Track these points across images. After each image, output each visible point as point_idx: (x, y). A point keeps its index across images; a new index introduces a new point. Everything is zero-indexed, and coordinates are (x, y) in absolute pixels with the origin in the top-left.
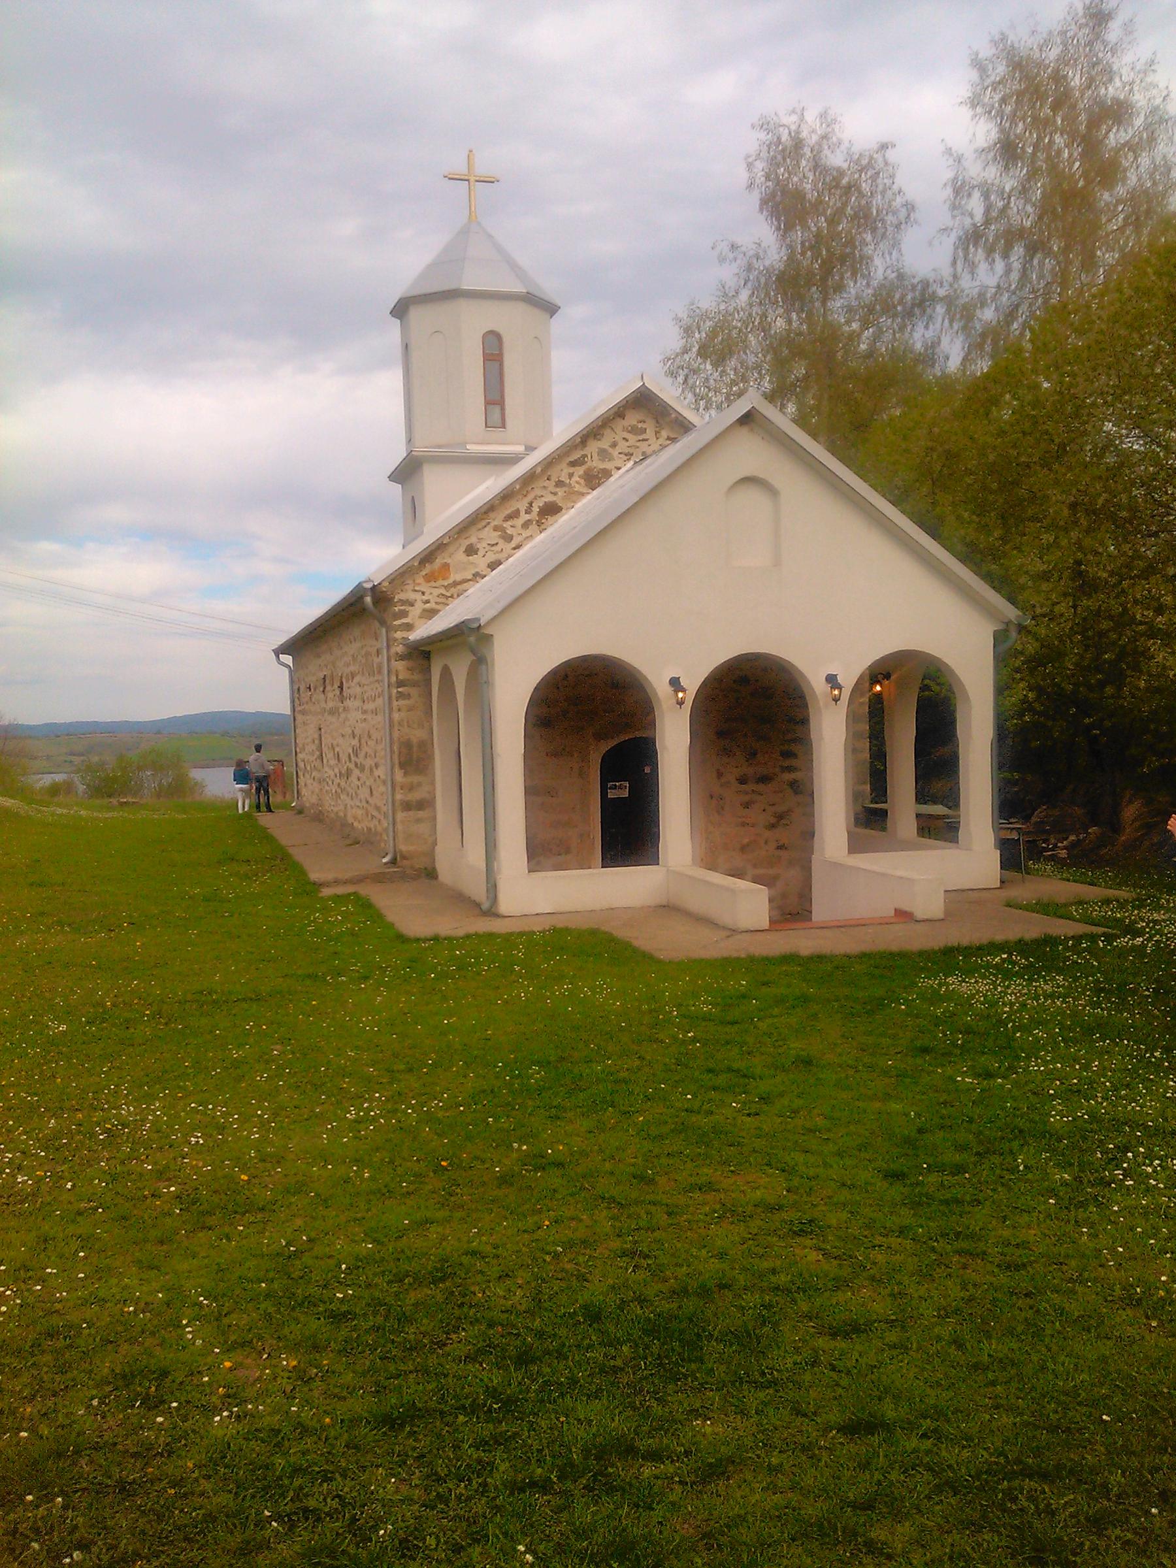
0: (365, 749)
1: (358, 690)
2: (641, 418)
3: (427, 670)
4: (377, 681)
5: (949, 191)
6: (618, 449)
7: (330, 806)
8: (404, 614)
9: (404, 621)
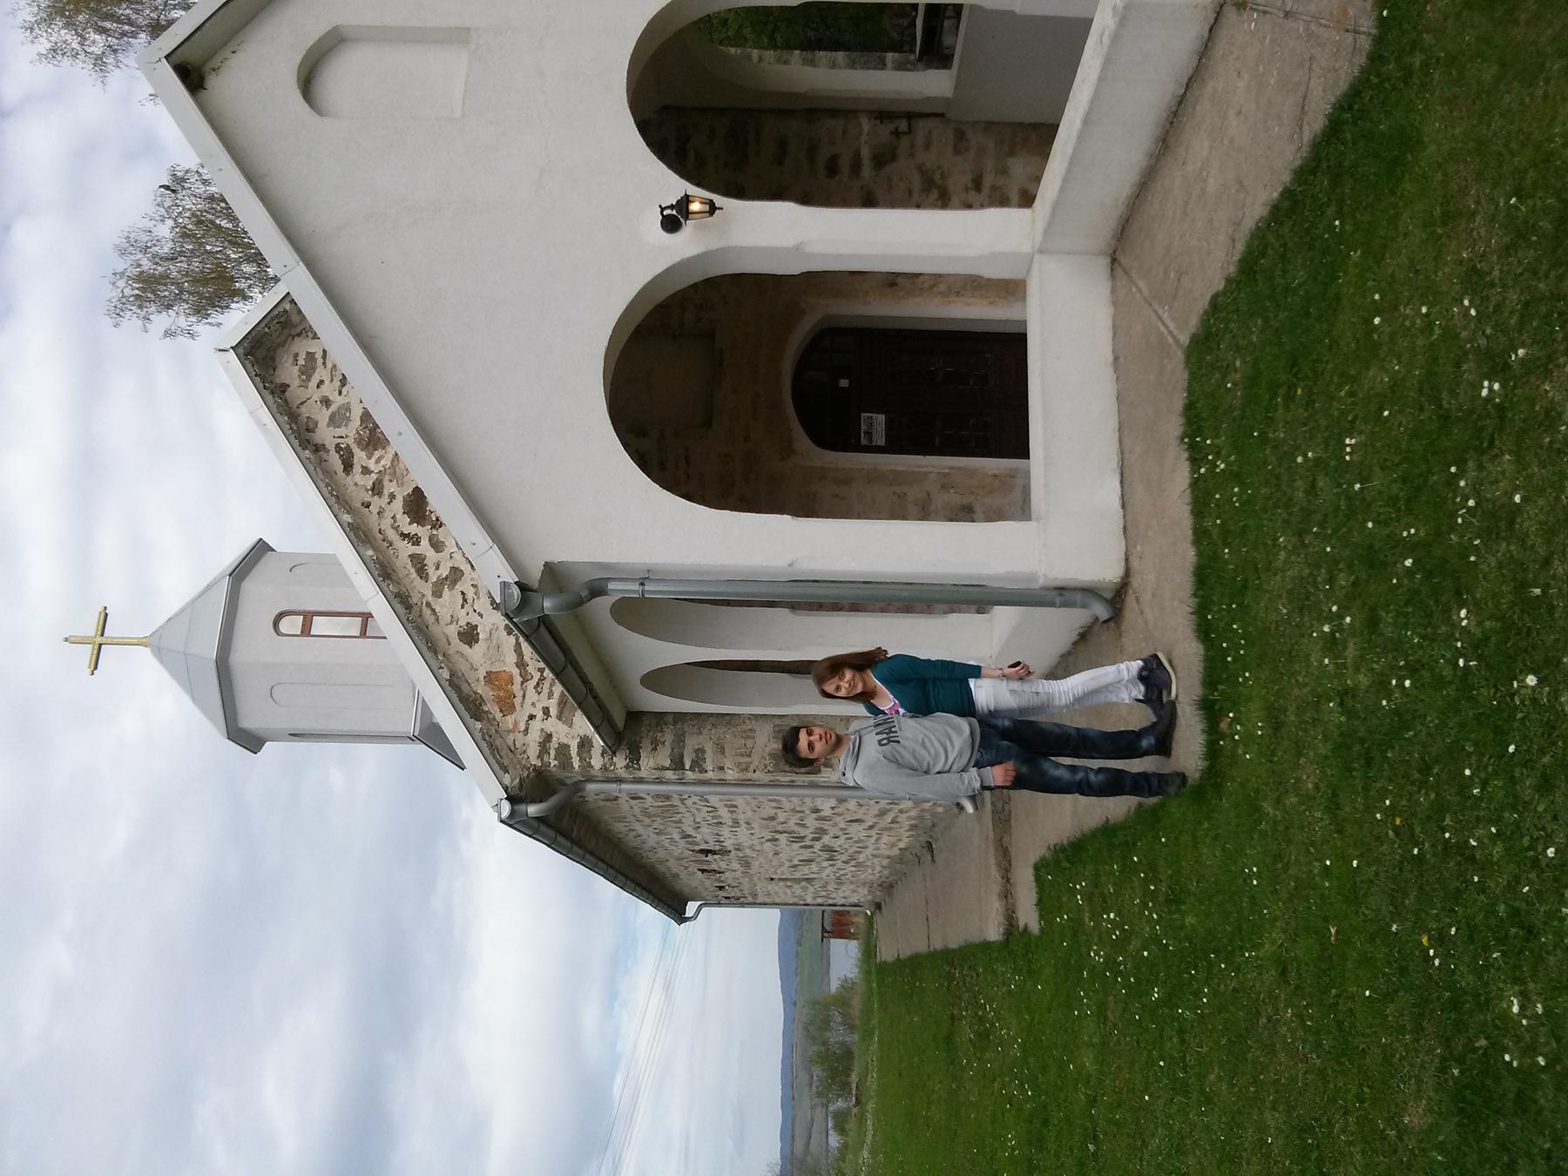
0: (791, 825)
1: (705, 830)
2: (291, 360)
4: (682, 801)
6: (334, 396)
7: (875, 871)
8: (563, 750)
9: (574, 751)
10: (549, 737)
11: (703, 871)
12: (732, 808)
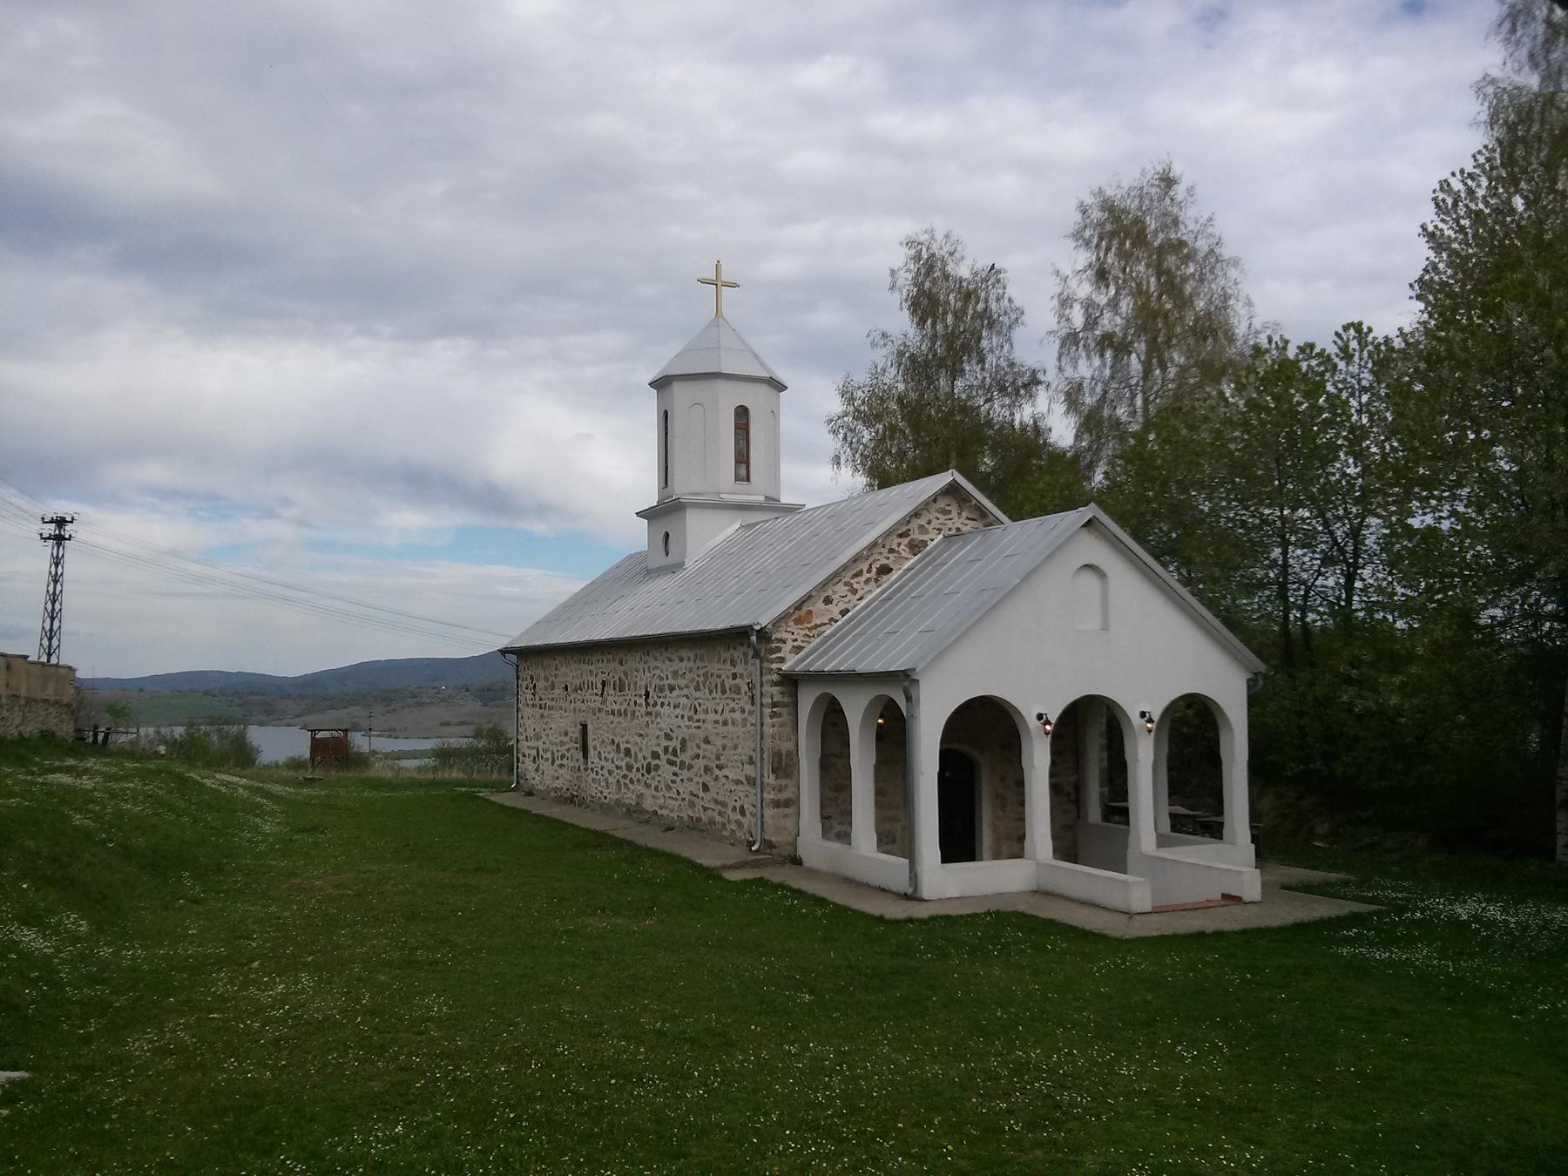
3: (795, 695)
5: (1055, 302)
8: (779, 650)
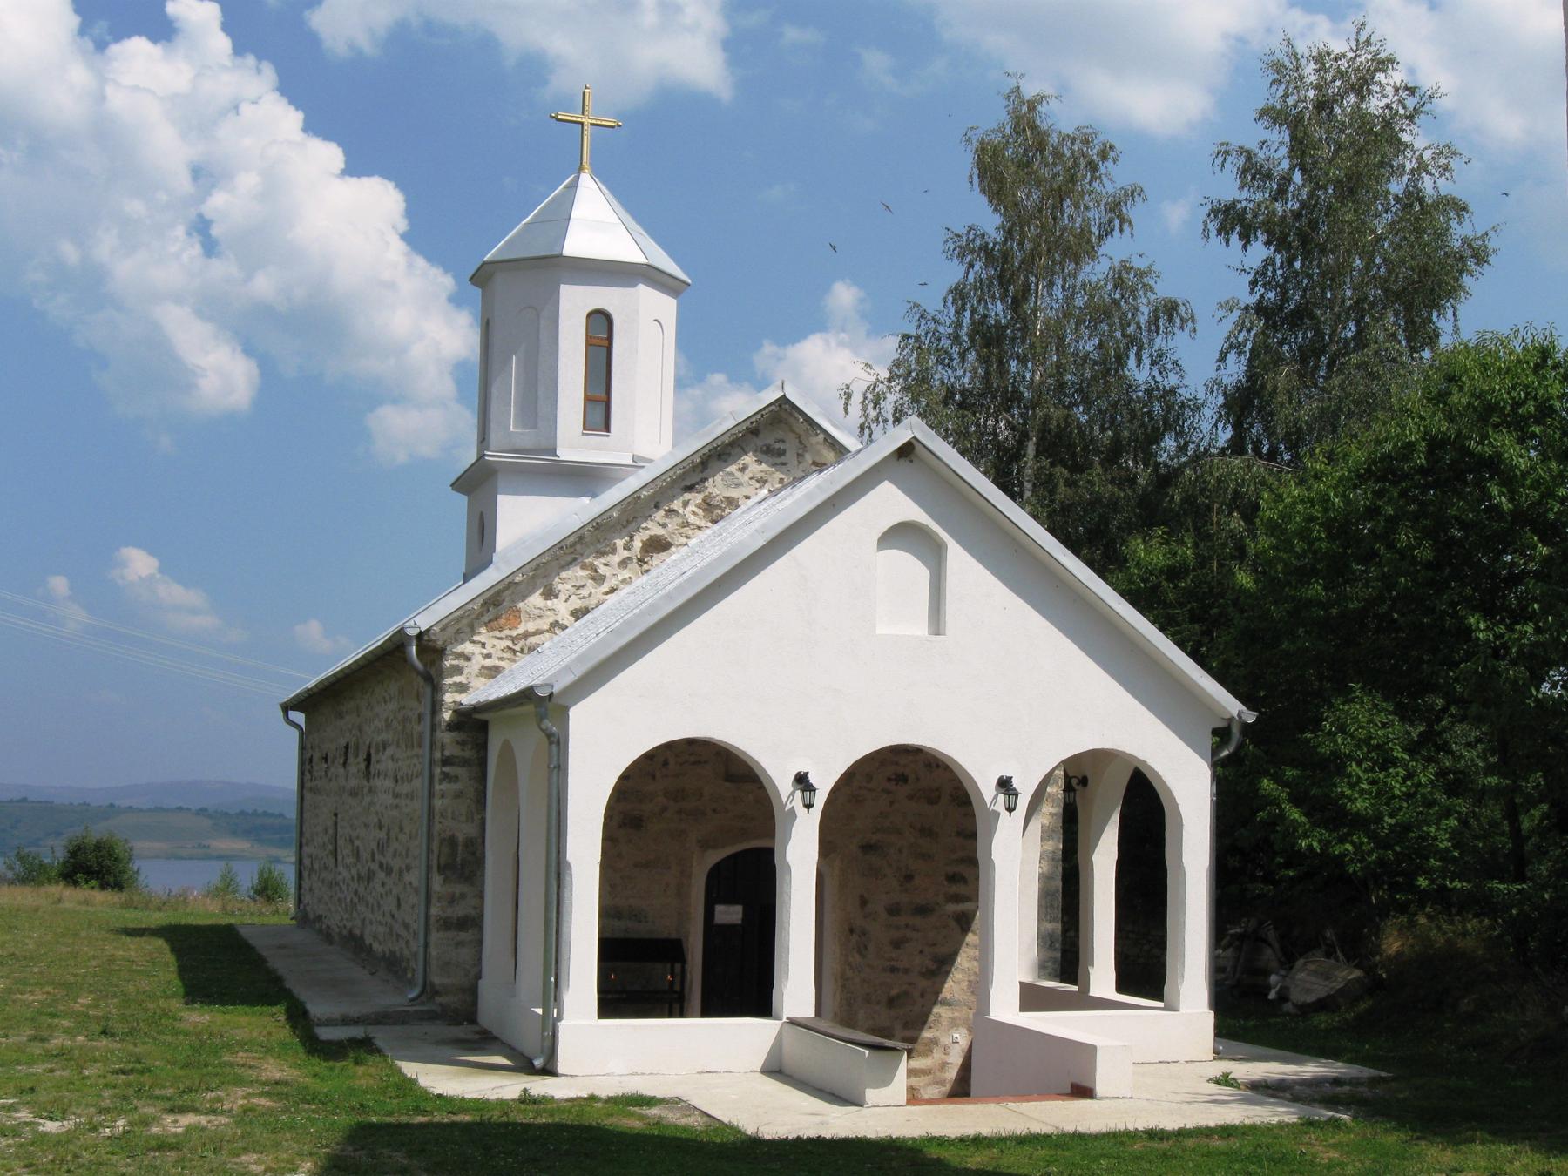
1: (390, 765)
6: (748, 474)
8: (458, 670)
9: (457, 679)
10: (468, 659)
11: (347, 747)
12: (411, 796)
